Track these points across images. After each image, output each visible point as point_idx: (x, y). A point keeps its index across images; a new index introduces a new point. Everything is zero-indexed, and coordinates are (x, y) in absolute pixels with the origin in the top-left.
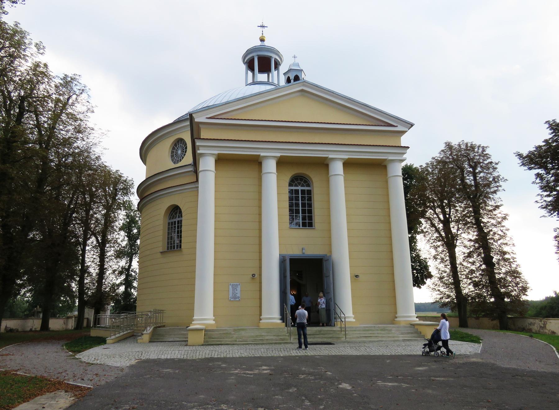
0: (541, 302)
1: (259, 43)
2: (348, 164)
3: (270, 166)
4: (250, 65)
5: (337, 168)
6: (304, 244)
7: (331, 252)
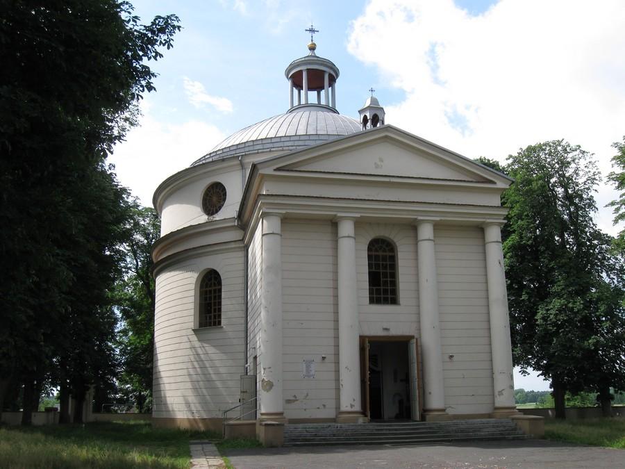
0: (176, 203)
1: (309, 53)
2: (438, 227)
3: (347, 228)
4: (296, 81)
5: (426, 231)
6: (387, 321)
7: (419, 329)
